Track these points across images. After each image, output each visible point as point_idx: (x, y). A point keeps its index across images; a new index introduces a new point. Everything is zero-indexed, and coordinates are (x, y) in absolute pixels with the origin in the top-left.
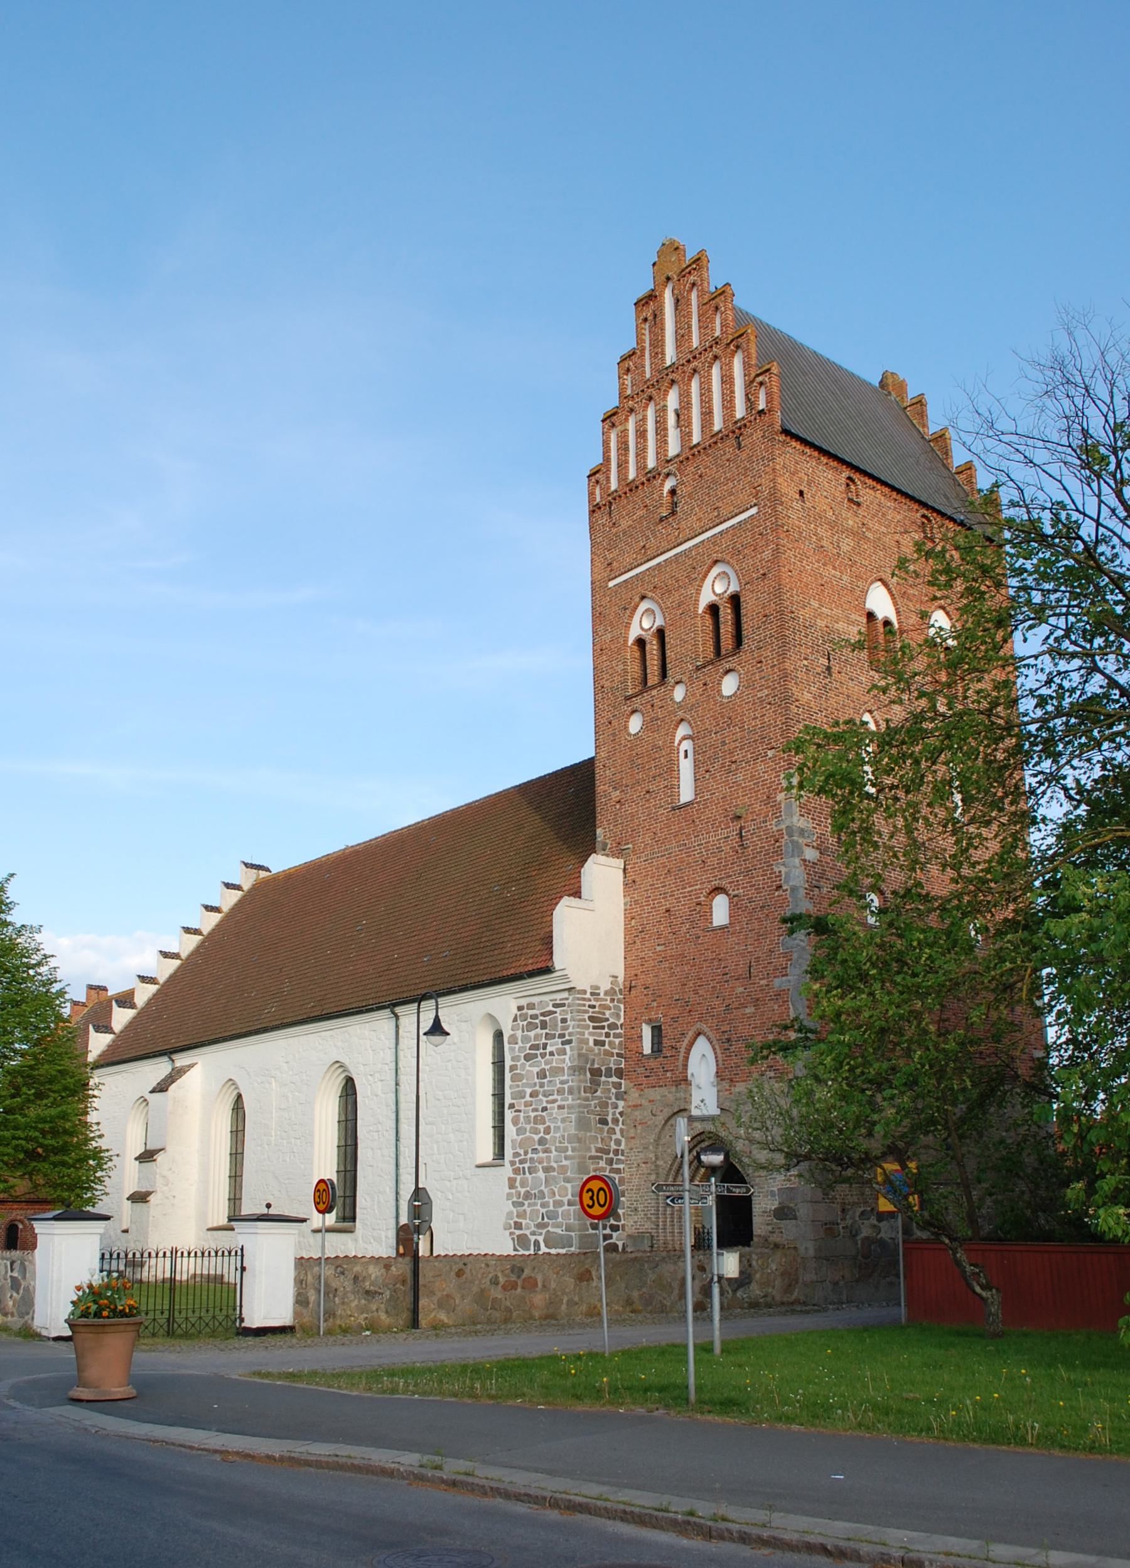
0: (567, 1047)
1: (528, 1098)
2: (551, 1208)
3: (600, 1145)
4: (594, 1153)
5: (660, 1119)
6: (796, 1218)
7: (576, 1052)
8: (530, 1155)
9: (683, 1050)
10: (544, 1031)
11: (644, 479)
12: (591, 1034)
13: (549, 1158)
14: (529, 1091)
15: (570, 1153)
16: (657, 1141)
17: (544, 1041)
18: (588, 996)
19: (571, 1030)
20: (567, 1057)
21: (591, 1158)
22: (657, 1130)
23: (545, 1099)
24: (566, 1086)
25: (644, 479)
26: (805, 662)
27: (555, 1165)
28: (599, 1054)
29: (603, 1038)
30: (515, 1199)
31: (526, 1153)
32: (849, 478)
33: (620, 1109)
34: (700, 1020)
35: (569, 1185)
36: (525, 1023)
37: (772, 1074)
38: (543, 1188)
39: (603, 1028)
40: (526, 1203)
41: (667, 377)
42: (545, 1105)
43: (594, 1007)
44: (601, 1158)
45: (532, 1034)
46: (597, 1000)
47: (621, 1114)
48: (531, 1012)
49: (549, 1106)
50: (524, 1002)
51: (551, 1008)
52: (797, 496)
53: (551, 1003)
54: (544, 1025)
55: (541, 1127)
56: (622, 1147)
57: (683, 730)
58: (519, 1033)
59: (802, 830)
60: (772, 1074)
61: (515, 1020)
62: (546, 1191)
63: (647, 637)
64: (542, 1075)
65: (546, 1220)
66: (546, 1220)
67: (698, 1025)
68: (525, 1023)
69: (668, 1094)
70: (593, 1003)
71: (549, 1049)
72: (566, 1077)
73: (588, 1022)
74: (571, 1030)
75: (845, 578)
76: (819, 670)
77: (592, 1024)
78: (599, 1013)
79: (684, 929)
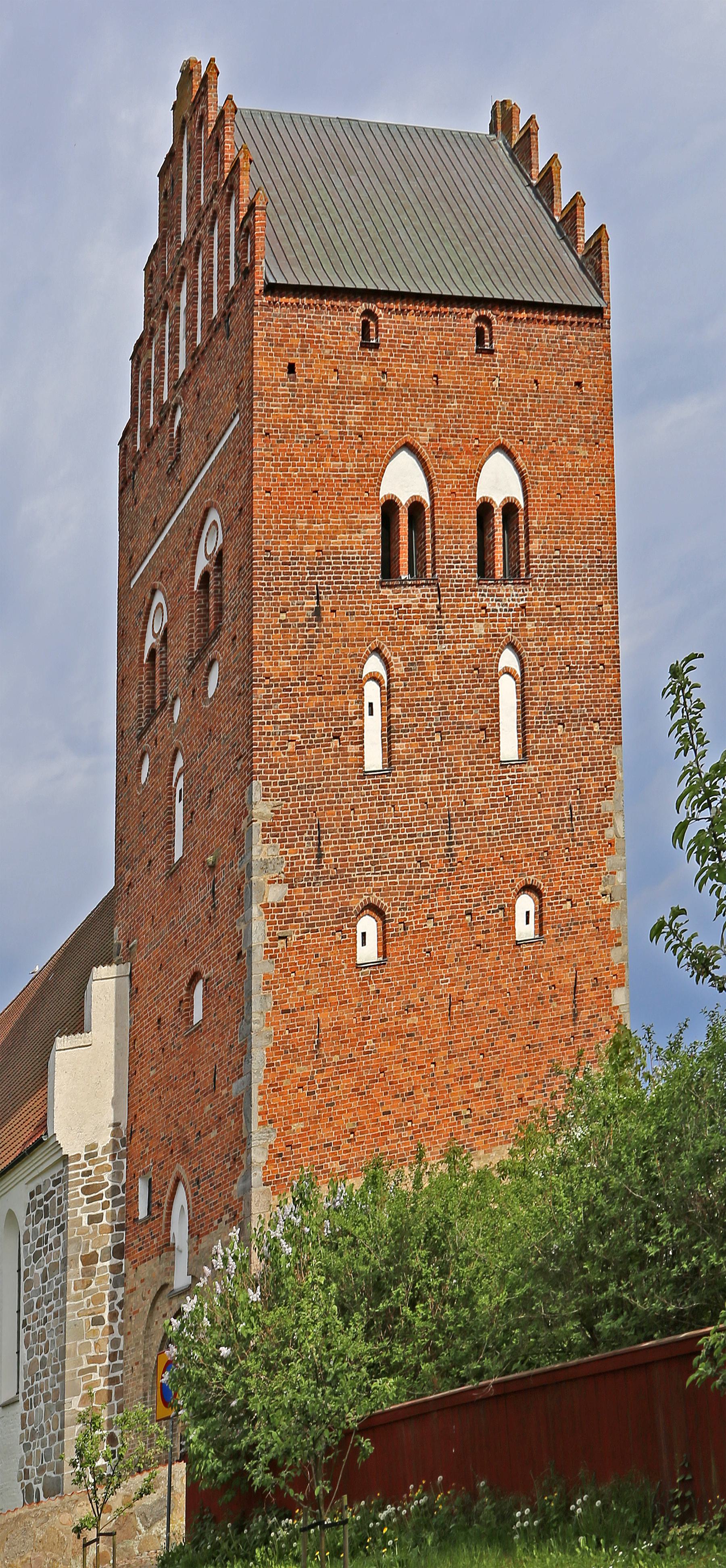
3: (93, 1353)
4: (85, 1365)
9: (165, 1206)
12: (84, 1211)
18: (82, 1160)
21: (82, 1372)
26: (283, 616)
28: (95, 1233)
29: (100, 1211)
32: (480, 319)
33: (120, 1298)
39: (100, 1197)
43: (89, 1173)
44: (93, 1369)
46: (92, 1163)
47: (121, 1305)
50: (32, 1187)
52: (285, 375)
56: (121, 1348)
59: (266, 863)
70: (89, 1168)
73: (81, 1196)
75: (349, 466)
76: (302, 619)
77: (86, 1197)
78: (96, 1179)
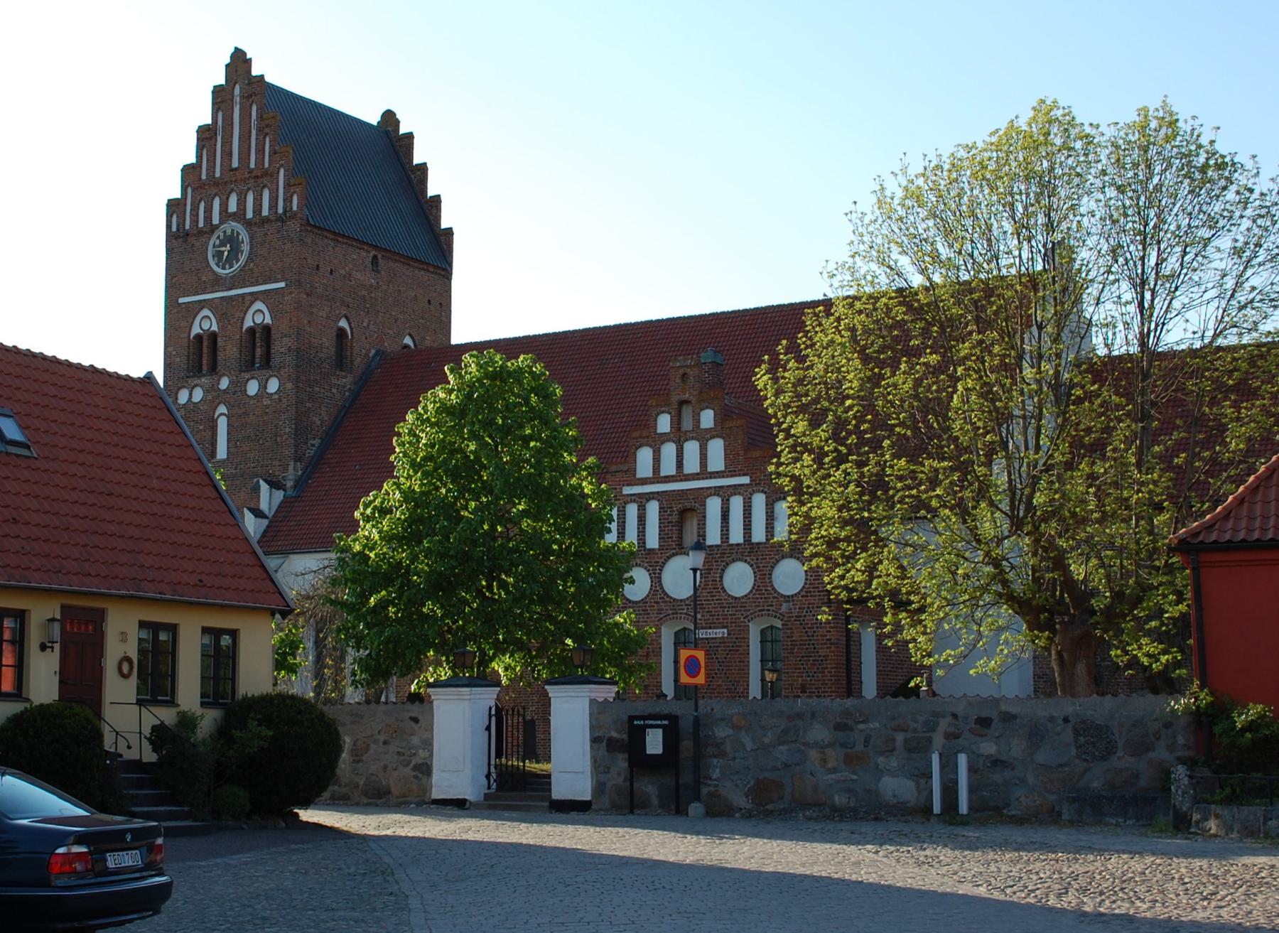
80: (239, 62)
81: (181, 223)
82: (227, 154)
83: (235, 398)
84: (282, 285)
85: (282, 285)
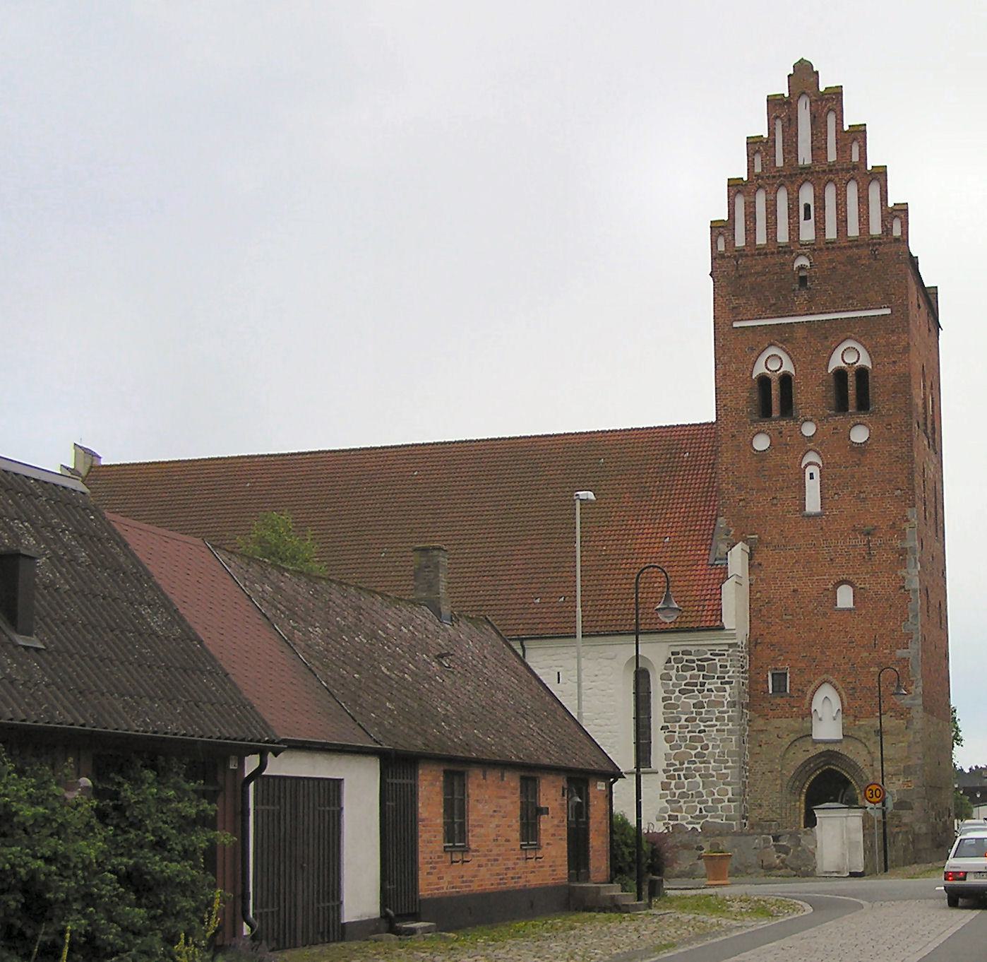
0: (727, 687)
1: (683, 722)
2: (710, 804)
5: (786, 741)
6: (912, 809)
7: (736, 691)
8: (686, 765)
10: (701, 673)
11: (776, 251)
13: (707, 769)
14: (684, 717)
15: (730, 764)
16: (783, 757)
17: (701, 680)
19: (730, 674)
20: (727, 694)
22: (783, 749)
23: (702, 724)
24: (726, 715)
25: (776, 251)
27: (714, 773)
30: (669, 798)
31: (682, 764)
34: (826, 672)
35: (729, 788)
36: (680, 665)
37: (892, 714)
38: (701, 789)
40: (682, 801)
41: (793, 176)
42: (702, 728)
45: (688, 674)
48: (686, 657)
49: (707, 729)
51: (708, 656)
53: (709, 653)
54: (701, 668)
55: (699, 745)
57: (812, 457)
58: (673, 673)
60: (892, 714)
61: (669, 661)
62: (704, 792)
63: (775, 378)
64: (699, 705)
65: (704, 813)
66: (704, 813)
67: (825, 676)
68: (680, 665)
69: (796, 724)
71: (707, 687)
72: (725, 708)
74: (730, 674)
79: (811, 607)
80: (803, 74)
81: (730, 242)
82: (842, 222)
83: (827, 444)
84: (888, 311)
85: (888, 311)
